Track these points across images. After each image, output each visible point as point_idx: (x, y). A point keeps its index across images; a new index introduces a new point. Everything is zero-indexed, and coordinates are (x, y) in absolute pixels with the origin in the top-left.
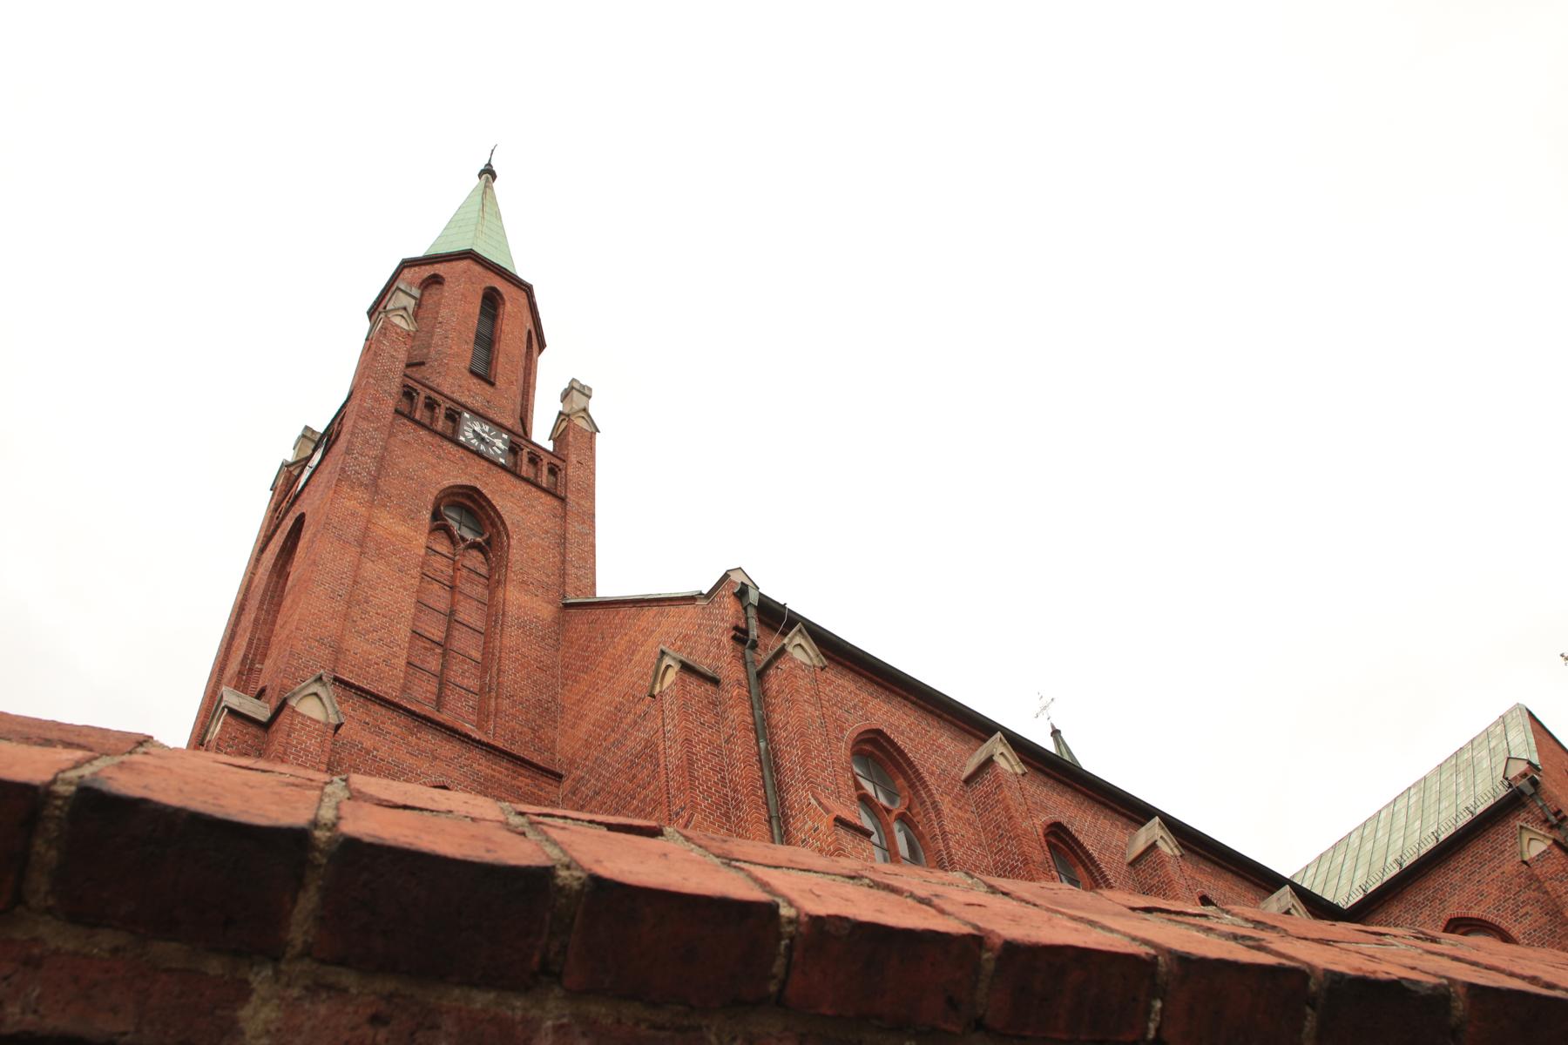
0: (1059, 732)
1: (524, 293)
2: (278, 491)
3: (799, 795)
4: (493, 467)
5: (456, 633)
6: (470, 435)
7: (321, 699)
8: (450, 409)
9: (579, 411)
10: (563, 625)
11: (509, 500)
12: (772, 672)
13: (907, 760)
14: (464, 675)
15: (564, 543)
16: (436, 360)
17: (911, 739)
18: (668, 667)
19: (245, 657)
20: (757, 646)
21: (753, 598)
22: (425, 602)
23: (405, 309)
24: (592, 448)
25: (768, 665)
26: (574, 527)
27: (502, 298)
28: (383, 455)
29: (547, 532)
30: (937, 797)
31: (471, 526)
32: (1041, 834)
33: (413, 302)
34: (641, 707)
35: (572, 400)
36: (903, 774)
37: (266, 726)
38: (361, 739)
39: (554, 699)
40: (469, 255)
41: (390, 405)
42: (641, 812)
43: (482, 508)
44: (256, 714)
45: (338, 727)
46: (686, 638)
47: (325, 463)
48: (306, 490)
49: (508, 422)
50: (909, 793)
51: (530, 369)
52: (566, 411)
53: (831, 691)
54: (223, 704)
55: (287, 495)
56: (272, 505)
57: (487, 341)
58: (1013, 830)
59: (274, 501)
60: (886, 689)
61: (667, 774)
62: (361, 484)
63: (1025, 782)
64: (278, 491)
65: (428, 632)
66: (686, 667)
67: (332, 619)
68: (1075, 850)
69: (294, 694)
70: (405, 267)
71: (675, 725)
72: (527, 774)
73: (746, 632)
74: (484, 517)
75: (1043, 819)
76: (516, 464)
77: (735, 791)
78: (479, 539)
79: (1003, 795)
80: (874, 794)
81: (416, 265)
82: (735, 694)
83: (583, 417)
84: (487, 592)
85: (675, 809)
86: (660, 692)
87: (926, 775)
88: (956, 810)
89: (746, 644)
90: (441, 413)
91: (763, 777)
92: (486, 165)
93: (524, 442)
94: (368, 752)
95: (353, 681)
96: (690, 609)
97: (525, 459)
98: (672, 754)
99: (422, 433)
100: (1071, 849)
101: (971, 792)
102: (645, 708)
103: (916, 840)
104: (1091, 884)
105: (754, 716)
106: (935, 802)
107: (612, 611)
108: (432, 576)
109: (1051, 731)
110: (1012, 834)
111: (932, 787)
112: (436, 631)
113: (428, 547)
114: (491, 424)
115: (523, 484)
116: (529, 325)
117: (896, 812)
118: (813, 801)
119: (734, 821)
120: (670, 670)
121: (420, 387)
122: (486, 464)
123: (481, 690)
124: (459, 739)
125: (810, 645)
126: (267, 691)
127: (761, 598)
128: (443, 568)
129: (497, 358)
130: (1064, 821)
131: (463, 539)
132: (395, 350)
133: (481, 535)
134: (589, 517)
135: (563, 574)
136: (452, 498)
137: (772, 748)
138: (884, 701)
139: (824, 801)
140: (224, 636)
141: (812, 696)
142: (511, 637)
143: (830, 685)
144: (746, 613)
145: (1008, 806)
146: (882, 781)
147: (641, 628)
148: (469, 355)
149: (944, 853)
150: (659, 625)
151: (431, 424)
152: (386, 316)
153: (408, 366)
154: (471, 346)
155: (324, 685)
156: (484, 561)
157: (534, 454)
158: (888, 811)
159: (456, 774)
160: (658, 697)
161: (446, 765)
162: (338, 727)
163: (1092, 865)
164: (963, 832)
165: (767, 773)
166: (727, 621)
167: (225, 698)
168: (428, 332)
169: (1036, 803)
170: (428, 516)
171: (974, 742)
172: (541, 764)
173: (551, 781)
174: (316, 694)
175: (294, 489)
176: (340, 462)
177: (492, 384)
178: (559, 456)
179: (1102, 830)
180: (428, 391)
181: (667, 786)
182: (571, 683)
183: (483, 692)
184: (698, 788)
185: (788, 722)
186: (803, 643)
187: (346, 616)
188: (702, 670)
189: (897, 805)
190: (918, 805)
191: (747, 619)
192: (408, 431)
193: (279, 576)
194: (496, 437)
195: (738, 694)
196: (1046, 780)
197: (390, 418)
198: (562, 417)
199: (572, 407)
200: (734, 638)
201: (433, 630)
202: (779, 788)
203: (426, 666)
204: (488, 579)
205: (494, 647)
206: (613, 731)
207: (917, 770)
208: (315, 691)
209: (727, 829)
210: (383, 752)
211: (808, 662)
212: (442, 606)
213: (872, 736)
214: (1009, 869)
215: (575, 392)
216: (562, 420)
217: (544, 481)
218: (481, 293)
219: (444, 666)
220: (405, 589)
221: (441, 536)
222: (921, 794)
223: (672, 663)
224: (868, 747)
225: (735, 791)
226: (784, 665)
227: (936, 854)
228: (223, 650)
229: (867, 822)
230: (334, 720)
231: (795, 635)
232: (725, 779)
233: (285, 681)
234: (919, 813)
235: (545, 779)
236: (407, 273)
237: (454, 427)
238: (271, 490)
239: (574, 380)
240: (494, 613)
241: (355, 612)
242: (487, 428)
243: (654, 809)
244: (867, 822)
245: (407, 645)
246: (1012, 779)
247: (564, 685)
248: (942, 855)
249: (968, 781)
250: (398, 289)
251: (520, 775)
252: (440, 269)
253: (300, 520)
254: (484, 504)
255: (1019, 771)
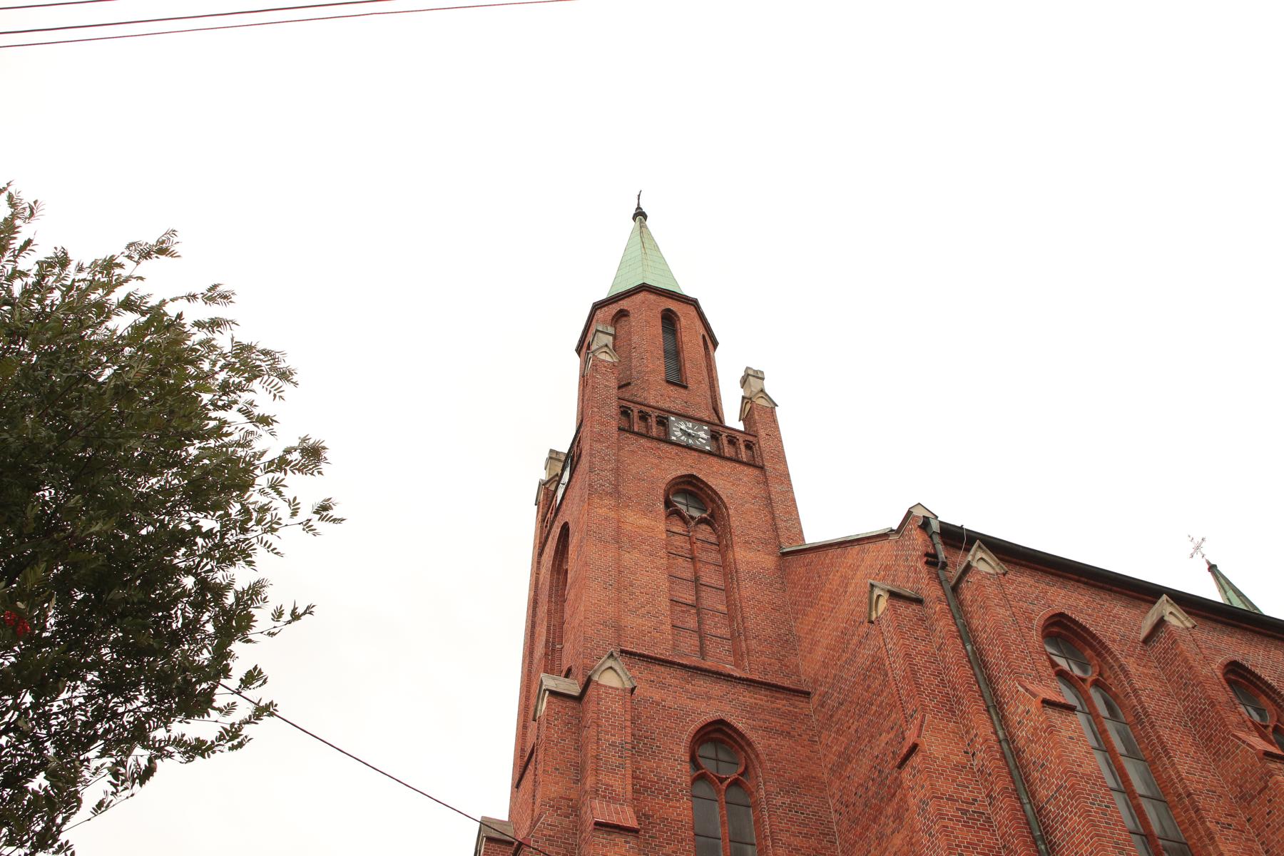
0: (1214, 566)
1: (692, 307)
2: (541, 505)
3: (1006, 685)
4: (702, 455)
5: (703, 594)
6: (679, 434)
7: (615, 671)
8: (659, 416)
9: (757, 393)
10: (785, 570)
11: (721, 478)
12: (963, 585)
13: (1090, 633)
14: (717, 627)
15: (771, 503)
16: (638, 379)
17: (1089, 615)
18: (879, 596)
19: (547, 641)
20: (947, 565)
21: (935, 526)
22: (674, 575)
23: (606, 346)
24: (775, 421)
25: (960, 579)
26: (775, 488)
27: (677, 316)
28: (618, 467)
29: (755, 497)
30: (1122, 660)
31: (696, 506)
32: (1221, 676)
33: (611, 338)
34: (863, 629)
35: (750, 385)
36: (1089, 646)
37: (579, 699)
38: (651, 695)
39: (790, 631)
40: (643, 288)
41: (614, 424)
42: (879, 715)
43: (701, 489)
44: (570, 691)
45: (633, 690)
46: (887, 568)
47: (574, 480)
48: (564, 503)
49: (705, 415)
50: (1098, 661)
51: (711, 365)
52: (748, 395)
53: (1015, 589)
54: (544, 687)
55: (549, 508)
56: (540, 517)
57: (674, 354)
58: (1194, 679)
59: (540, 513)
60: (1060, 576)
61: (896, 684)
62: (607, 494)
63: (1198, 634)
64: (541, 505)
65: (681, 597)
66: (893, 595)
67: (609, 604)
68: (1255, 683)
69: (595, 671)
70: (597, 309)
71: (895, 643)
72: (782, 696)
73: (935, 556)
74: (704, 496)
75: (1221, 660)
76: (719, 448)
77: (955, 689)
78: (704, 515)
79: (1180, 649)
80: (1068, 669)
81: (604, 306)
82: (937, 609)
83: (762, 397)
84: (719, 556)
85: (909, 712)
86: (877, 618)
87: (1108, 643)
88: (1141, 669)
89: (937, 565)
90: (652, 421)
91: (975, 675)
92: (637, 209)
93: (721, 429)
94: (658, 704)
95: (634, 650)
96: (885, 544)
97: (725, 442)
98: (897, 667)
99: (642, 441)
100: (1251, 682)
101: (1150, 650)
102: (865, 630)
103: (1110, 699)
104: (1276, 710)
105: (957, 625)
106: (1121, 665)
107: (821, 554)
108: (675, 553)
109: (1207, 567)
110: (1194, 681)
111: (1117, 653)
112: (689, 597)
113: (667, 531)
114: (691, 420)
115: (728, 463)
116: (702, 331)
117: (1090, 680)
118: (1020, 688)
119: (958, 715)
120: (881, 599)
121: (632, 405)
122: (696, 454)
123: (732, 636)
124: (724, 679)
125: (990, 556)
126: (573, 670)
127: (942, 525)
128: (683, 545)
129: (684, 364)
130: (1238, 659)
131: (692, 518)
132: (607, 381)
133: (705, 511)
134: (785, 477)
135: (776, 529)
136: (676, 487)
137: (976, 648)
138: (1060, 588)
139: (1029, 687)
140: (527, 626)
141: (1001, 600)
142: (747, 589)
143: (1012, 584)
144: (932, 540)
145: (1186, 657)
146: (1071, 655)
147: (848, 565)
148: (662, 368)
149: (1139, 707)
150: (863, 560)
151: (647, 432)
152: (594, 355)
153: (620, 387)
154: (662, 360)
155: (616, 659)
156: (712, 531)
157: (731, 436)
158: (1083, 680)
159: (728, 708)
160: (876, 622)
161: (719, 702)
162: (633, 690)
163: (1274, 693)
164: (1151, 687)
165: (977, 670)
166: (917, 550)
167: (544, 683)
168: (626, 357)
169: (1210, 648)
170: (662, 506)
171: (1144, 605)
172: (791, 686)
173: (802, 699)
174: (611, 668)
175: (554, 502)
176: (587, 479)
177: (685, 387)
178: (751, 433)
179: (1275, 660)
180: (639, 406)
181: (899, 694)
182: (801, 617)
183: (734, 637)
184: (924, 692)
185: (986, 626)
186: (984, 556)
187: (619, 600)
188: (907, 594)
189: (1090, 673)
190: (1108, 670)
191: (934, 545)
192: (633, 443)
193: (559, 573)
194: (698, 430)
195: (941, 609)
196: (1214, 625)
197: (616, 435)
198: (746, 401)
199: (752, 391)
200: (927, 563)
201: (685, 596)
202: (990, 681)
203: (687, 626)
204: (718, 545)
205: (735, 600)
206: (844, 651)
207: (1100, 641)
208: (610, 665)
209: (954, 722)
210: (669, 702)
211: (992, 572)
212: (688, 574)
213: (1056, 619)
214: (1199, 712)
215: (751, 377)
216: (746, 403)
217: (744, 456)
218: (659, 316)
219: (700, 623)
220: (658, 569)
221: (675, 518)
222: (1107, 661)
223: (882, 593)
224: (1055, 629)
225: (955, 689)
226: (972, 578)
227: (1132, 709)
228: (529, 637)
229: (1069, 697)
230: (628, 685)
231: (976, 551)
232: (944, 680)
233: (585, 661)
234: (1109, 677)
235: (797, 698)
236: (599, 314)
237: (665, 430)
238: (536, 505)
239: (747, 368)
240: (728, 570)
241: (625, 595)
242: (690, 425)
243: (891, 711)
244: (1069, 697)
245: (669, 613)
246: (1185, 633)
247: (796, 619)
248: (1137, 709)
249: (1146, 641)
250: (597, 331)
251: (777, 698)
252: (624, 304)
253: (565, 528)
254: (702, 486)
255: (1189, 625)
